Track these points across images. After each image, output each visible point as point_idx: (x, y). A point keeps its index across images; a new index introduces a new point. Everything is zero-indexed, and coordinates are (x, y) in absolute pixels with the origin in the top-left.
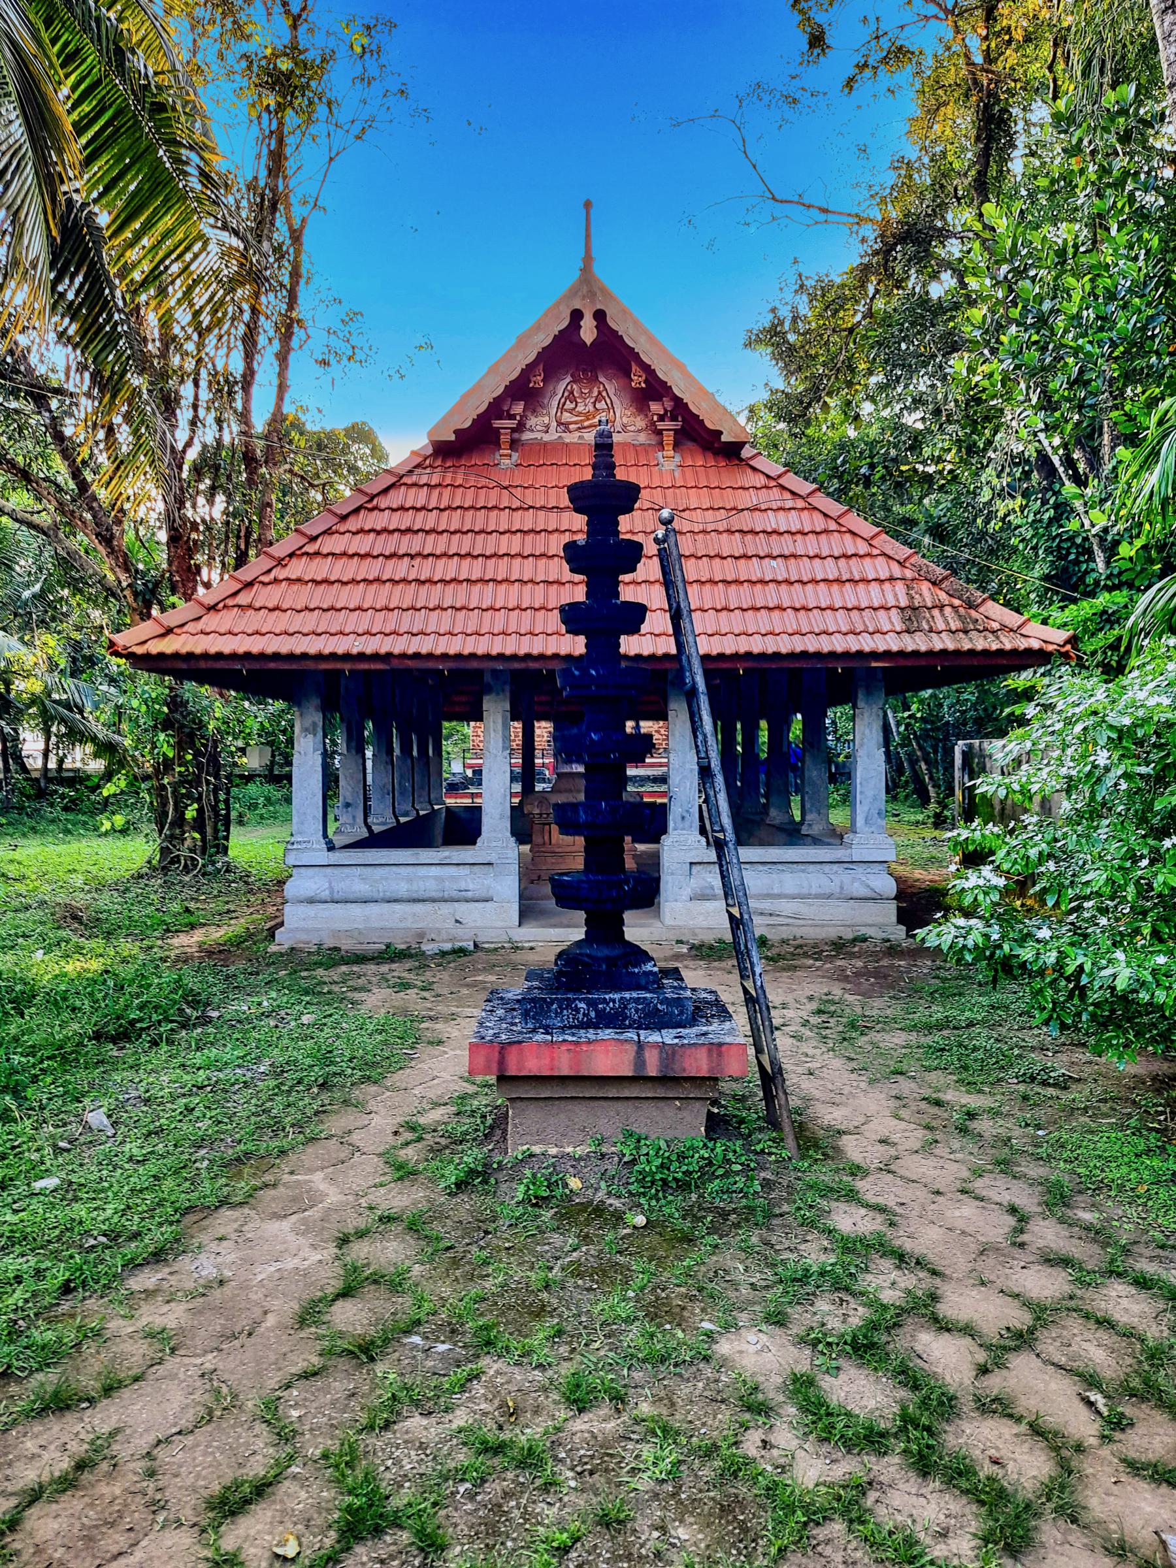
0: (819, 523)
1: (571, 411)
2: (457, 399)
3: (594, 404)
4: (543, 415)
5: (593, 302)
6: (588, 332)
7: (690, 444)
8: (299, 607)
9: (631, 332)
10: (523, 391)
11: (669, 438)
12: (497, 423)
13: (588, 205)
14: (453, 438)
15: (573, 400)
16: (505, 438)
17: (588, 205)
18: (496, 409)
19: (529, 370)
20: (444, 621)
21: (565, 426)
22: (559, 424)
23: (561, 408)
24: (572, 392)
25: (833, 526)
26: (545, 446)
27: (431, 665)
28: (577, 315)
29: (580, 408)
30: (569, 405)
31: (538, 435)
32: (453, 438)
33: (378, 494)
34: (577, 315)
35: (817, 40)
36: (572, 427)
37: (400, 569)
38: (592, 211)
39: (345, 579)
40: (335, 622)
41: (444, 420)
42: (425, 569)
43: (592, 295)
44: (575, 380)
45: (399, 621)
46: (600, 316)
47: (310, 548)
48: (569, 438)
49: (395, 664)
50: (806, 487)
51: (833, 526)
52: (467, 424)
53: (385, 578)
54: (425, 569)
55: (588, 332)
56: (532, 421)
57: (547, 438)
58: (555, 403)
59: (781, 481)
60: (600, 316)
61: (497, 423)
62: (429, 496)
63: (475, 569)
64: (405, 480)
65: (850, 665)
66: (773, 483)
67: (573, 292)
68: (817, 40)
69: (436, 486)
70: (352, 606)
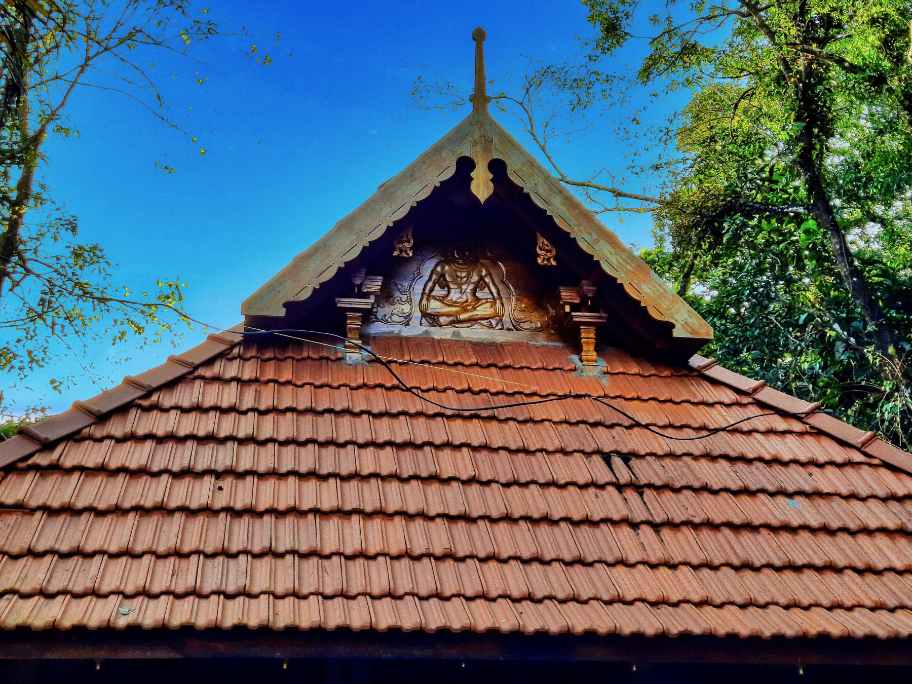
0: (839, 454)
1: (442, 299)
2: (288, 261)
3: (474, 292)
4: (401, 302)
5: (487, 150)
6: (481, 186)
7: (611, 350)
8: (15, 550)
9: (540, 190)
10: (381, 261)
11: (588, 336)
12: (345, 302)
13: (479, 37)
14: (282, 313)
15: (444, 285)
16: (353, 323)
17: (479, 37)
18: (345, 281)
19: (395, 232)
20: (284, 575)
21: (433, 319)
22: (425, 315)
23: (428, 295)
24: (442, 275)
25: (858, 457)
26: (402, 343)
27: (260, 651)
28: (465, 165)
29: (455, 295)
30: (438, 292)
31: (396, 329)
32: (282, 313)
33: (159, 388)
34: (465, 165)
35: (612, 29)
36: (442, 320)
37: (201, 493)
38: (486, 45)
39: (102, 506)
40: (81, 575)
41: (272, 288)
42: (242, 494)
43: (487, 143)
44: (447, 259)
45: (201, 574)
46: (497, 168)
47: (43, 460)
48: (437, 333)
49: (195, 650)
50: (802, 406)
51: (858, 457)
52: (305, 295)
53: (173, 505)
54: (242, 494)
55: (481, 186)
56: (384, 311)
57: (406, 332)
58: (418, 288)
59: (758, 396)
60: (497, 168)
61: (345, 302)
62: (241, 395)
63: (328, 495)
64: (202, 372)
65: (113, 656)
66: (745, 400)
67: (459, 135)
68: (612, 29)
69: (251, 382)
70: (113, 548)
